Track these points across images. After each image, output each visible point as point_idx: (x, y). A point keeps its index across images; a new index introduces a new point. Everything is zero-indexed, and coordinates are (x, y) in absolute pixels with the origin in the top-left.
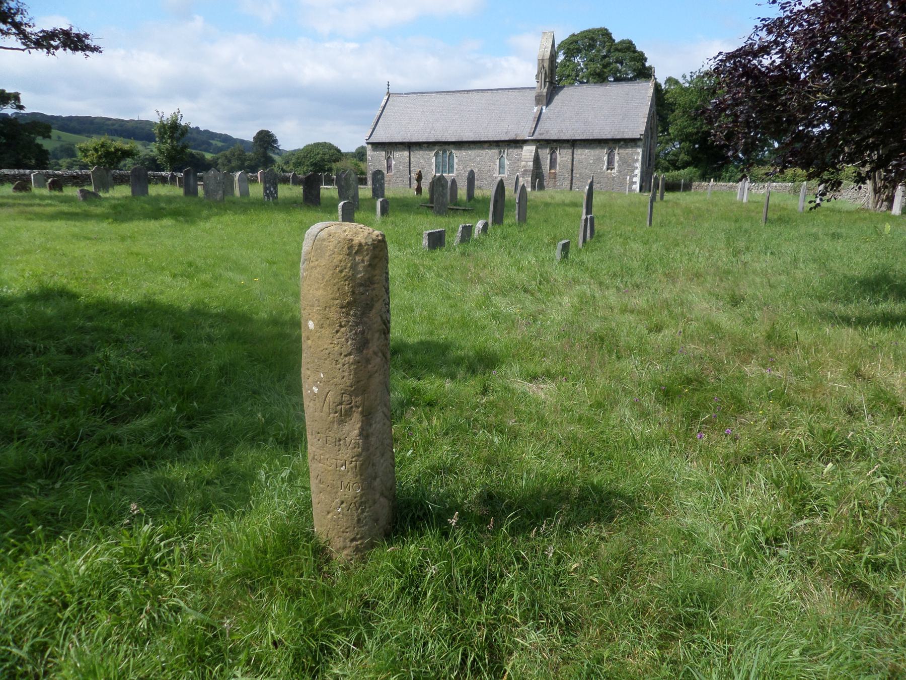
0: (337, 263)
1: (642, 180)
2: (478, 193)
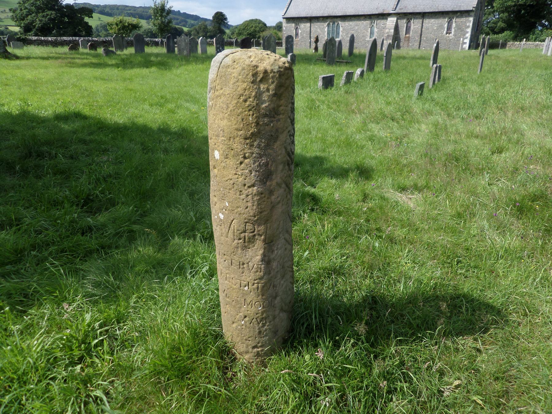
0: (241, 92)
1: (471, 41)
2: (356, 51)
